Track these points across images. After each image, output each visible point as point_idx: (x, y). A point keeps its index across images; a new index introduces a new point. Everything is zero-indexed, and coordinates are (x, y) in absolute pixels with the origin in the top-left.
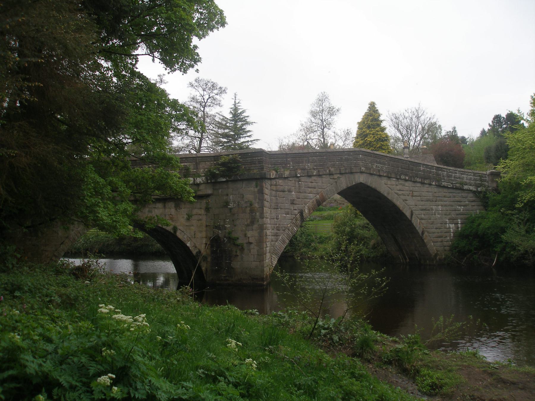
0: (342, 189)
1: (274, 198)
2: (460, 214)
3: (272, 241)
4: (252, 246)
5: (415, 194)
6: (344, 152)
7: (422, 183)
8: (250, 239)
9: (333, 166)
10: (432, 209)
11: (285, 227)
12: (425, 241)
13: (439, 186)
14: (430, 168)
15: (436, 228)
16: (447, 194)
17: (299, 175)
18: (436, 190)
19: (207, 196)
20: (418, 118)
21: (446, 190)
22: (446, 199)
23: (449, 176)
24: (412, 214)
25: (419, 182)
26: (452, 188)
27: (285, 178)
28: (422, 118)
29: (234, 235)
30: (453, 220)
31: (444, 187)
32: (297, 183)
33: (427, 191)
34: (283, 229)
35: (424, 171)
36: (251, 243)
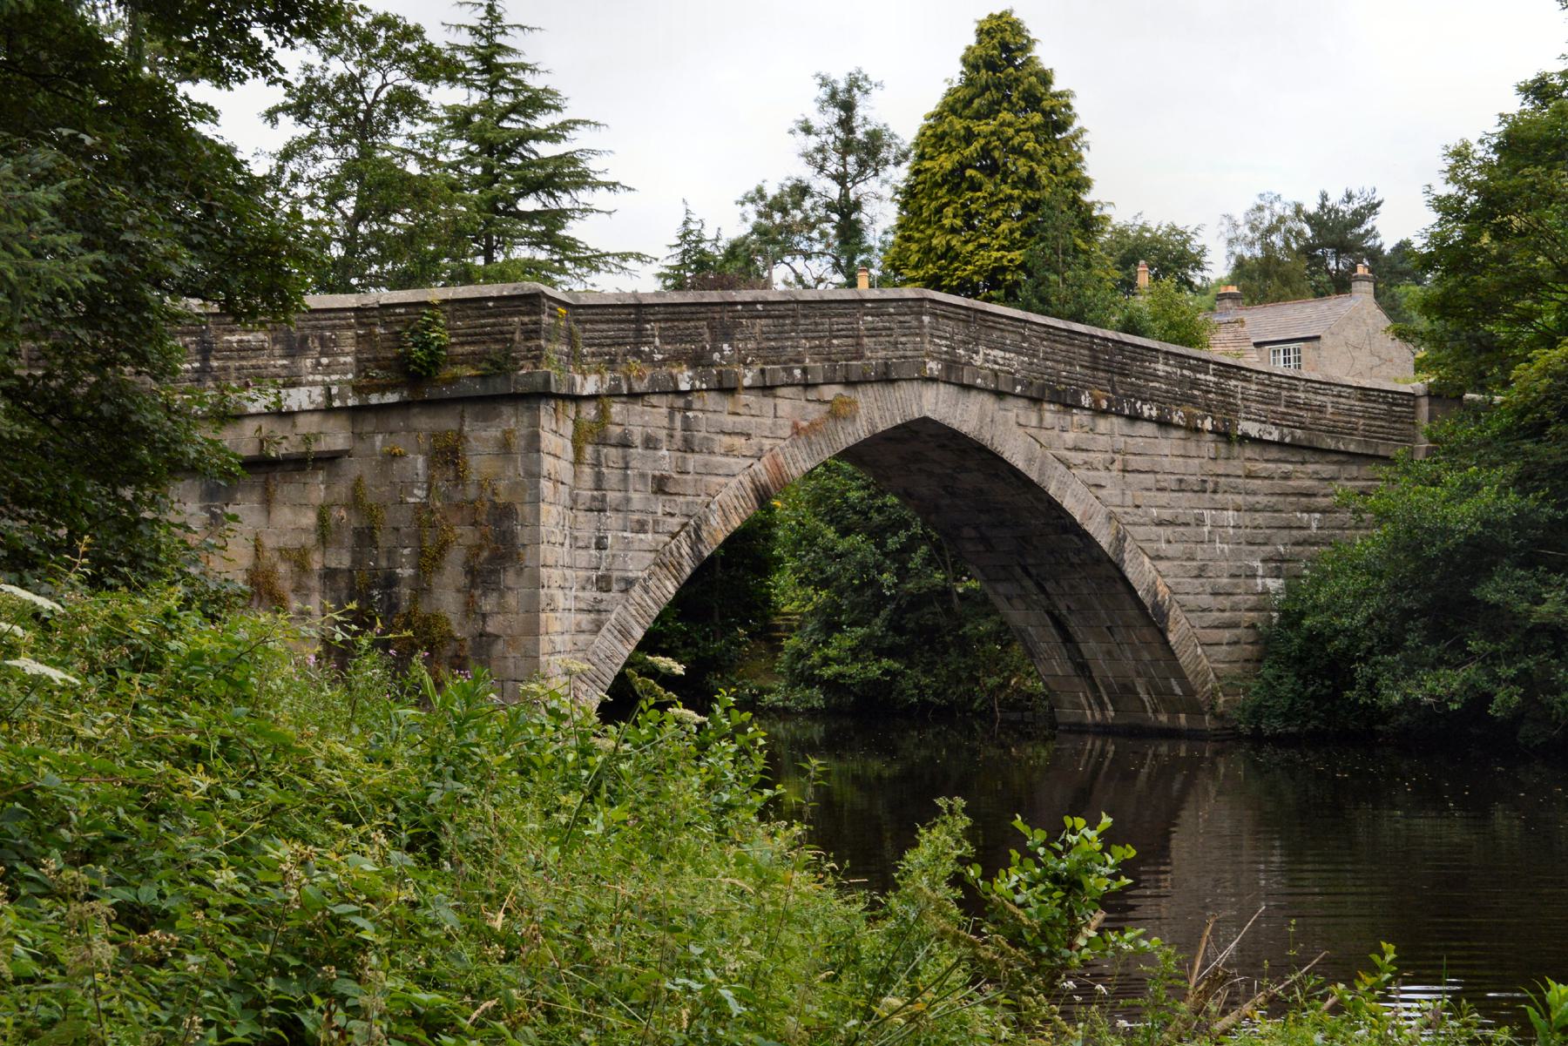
0: (851, 441)
5: (1135, 462)
7: (1163, 423)
15: (1215, 594)
17: (684, 386)
19: (330, 460)
21: (1249, 452)
24: (1120, 540)
25: (1150, 420)
31: (1245, 438)
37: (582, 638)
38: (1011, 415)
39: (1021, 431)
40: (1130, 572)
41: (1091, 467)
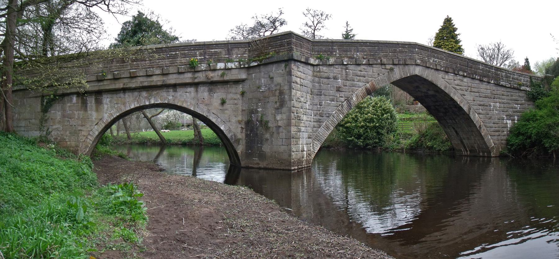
0: (395, 80)
1: (316, 84)
2: (516, 112)
3: (314, 127)
4: (281, 130)
5: (473, 90)
6: (398, 44)
7: (481, 81)
8: (279, 122)
9: (386, 56)
10: (490, 106)
11: (329, 114)
12: (483, 134)
13: (498, 85)
14: (489, 68)
15: (494, 123)
16: (505, 93)
17: (345, 63)
18: (494, 88)
19: (243, 81)
20: (499, 49)
21: (503, 89)
22: (503, 97)
23: (507, 77)
24: (470, 109)
25: (478, 79)
26: (510, 88)
27: (329, 65)
28: (502, 50)
29: (265, 119)
30: (509, 117)
31: (502, 86)
32: (344, 71)
33: (485, 88)
34: (327, 115)
35: (482, 70)
36: (280, 127)
37: (315, 129)
38: (440, 76)
39: (443, 80)
40: (472, 116)
41: (462, 90)
